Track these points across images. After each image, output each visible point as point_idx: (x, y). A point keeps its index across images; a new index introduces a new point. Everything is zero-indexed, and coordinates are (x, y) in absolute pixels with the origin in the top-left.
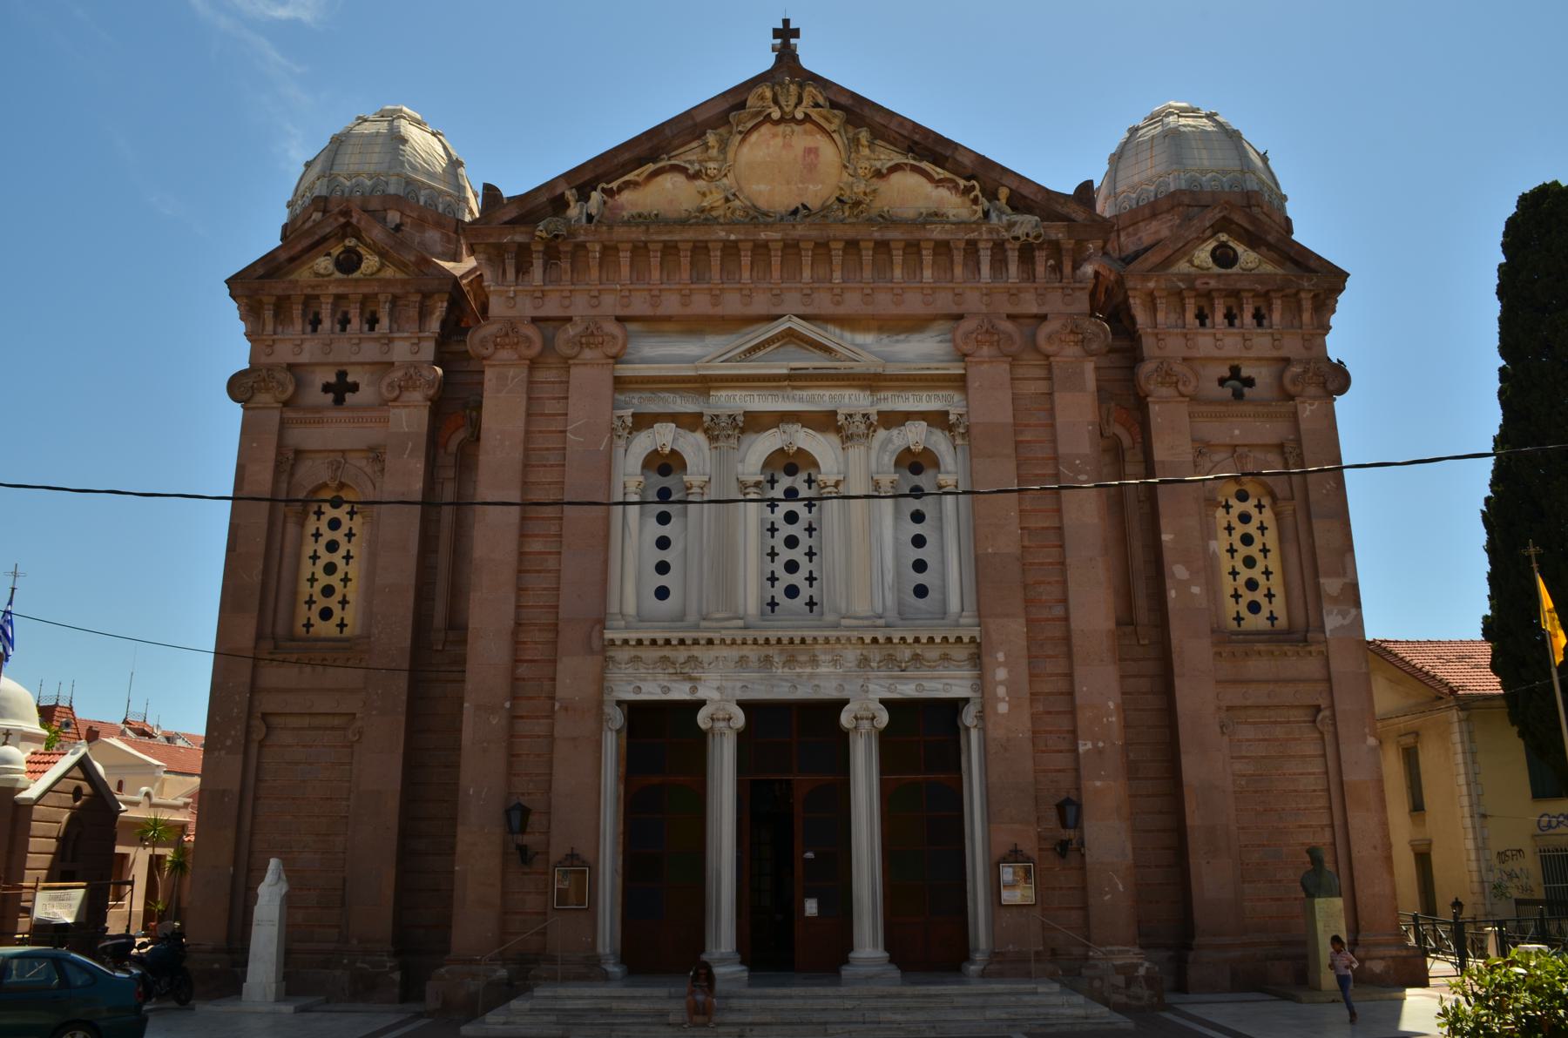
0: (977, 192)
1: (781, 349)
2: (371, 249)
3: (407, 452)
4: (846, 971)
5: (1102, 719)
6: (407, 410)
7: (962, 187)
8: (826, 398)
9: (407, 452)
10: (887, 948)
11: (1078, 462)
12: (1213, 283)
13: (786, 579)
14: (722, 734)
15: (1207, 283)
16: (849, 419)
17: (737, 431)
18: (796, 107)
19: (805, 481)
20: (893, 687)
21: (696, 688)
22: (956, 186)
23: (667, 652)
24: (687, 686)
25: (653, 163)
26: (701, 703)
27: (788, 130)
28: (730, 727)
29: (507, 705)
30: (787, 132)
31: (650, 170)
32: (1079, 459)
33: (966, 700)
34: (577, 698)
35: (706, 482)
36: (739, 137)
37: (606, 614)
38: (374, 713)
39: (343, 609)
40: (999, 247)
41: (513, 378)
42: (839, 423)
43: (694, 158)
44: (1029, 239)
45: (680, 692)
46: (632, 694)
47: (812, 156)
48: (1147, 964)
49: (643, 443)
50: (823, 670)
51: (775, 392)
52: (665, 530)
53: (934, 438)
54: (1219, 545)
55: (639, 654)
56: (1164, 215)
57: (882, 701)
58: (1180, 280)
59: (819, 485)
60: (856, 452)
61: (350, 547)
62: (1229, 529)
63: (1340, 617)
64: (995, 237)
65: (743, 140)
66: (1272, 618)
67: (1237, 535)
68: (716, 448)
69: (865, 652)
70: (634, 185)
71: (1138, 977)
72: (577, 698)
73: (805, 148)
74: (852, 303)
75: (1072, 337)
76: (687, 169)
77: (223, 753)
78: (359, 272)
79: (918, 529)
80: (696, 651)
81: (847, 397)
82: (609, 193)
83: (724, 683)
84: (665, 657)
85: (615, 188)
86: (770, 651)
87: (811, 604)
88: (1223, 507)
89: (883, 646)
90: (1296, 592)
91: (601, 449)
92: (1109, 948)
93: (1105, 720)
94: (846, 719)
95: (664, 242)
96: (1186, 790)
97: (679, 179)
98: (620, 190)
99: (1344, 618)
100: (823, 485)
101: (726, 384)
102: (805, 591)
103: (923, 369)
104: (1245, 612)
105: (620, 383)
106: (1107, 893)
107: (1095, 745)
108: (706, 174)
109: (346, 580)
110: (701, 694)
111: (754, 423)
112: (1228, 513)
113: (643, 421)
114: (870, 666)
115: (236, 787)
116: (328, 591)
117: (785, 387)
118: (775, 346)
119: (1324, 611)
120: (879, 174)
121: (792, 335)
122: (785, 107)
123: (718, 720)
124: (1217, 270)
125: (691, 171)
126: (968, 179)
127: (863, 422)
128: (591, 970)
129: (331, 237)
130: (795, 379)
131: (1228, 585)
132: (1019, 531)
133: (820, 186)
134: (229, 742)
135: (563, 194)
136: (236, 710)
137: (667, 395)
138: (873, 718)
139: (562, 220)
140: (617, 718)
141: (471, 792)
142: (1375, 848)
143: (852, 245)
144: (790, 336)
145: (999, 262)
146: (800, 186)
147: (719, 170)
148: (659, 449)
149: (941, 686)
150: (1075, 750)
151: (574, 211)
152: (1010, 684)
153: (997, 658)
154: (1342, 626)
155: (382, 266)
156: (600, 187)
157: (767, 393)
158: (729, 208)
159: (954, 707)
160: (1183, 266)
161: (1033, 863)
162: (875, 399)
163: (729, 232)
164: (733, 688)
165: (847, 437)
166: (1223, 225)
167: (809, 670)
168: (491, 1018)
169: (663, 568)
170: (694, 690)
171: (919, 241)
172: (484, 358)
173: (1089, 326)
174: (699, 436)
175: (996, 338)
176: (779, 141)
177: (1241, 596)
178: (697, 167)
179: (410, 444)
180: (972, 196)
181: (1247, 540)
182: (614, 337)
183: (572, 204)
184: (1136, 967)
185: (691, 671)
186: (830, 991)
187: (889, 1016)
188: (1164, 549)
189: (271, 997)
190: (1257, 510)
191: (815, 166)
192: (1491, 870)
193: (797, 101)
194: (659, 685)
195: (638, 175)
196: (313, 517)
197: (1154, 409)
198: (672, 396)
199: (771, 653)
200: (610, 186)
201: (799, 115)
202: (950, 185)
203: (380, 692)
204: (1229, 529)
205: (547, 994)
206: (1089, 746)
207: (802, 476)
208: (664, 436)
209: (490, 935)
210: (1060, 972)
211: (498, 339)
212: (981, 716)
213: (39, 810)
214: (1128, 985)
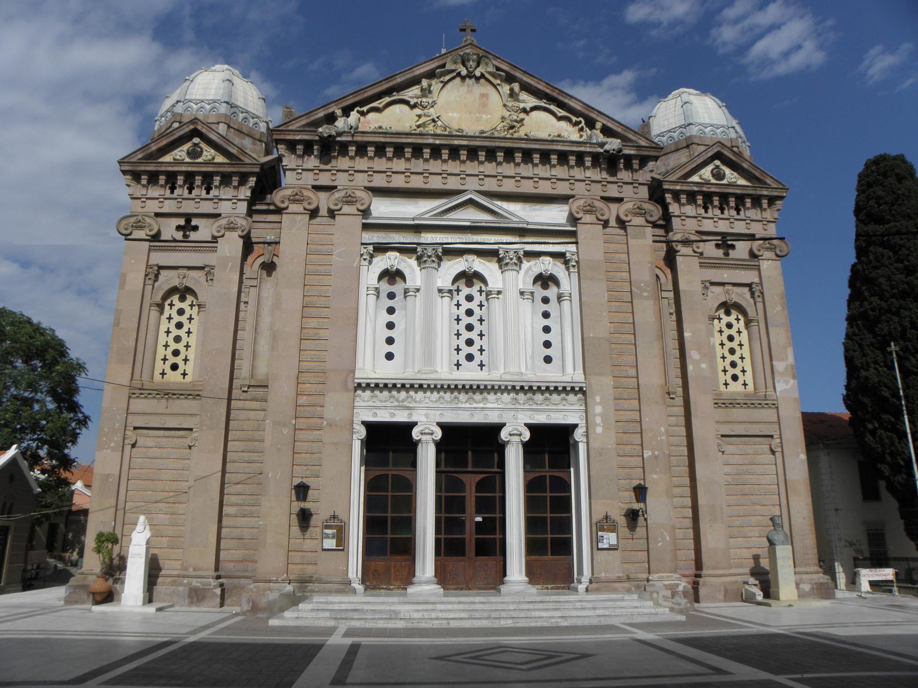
0: (583, 124)
4: (503, 588)
7: (574, 121)
11: (642, 285)
12: (713, 189)
13: (466, 350)
18: (476, 68)
19: (478, 291)
24: (406, 413)
25: (389, 97)
26: (414, 424)
32: (643, 283)
34: (337, 419)
38: (205, 428)
39: (185, 364)
42: (500, 256)
47: (485, 98)
48: (683, 584)
52: (391, 318)
54: (717, 339)
57: (527, 425)
60: (510, 275)
61: (190, 326)
62: (721, 332)
63: (784, 384)
66: (745, 385)
67: (725, 335)
70: (377, 110)
71: (679, 591)
72: (337, 419)
77: (109, 451)
78: (201, 158)
79: (546, 322)
82: (363, 114)
85: (365, 111)
88: (717, 319)
90: (760, 369)
91: (355, 266)
92: (661, 574)
94: (504, 435)
96: (698, 483)
97: (405, 108)
98: (369, 111)
99: (787, 385)
102: (478, 358)
104: (730, 381)
106: (660, 541)
107: (653, 453)
109: (187, 346)
112: (720, 322)
113: (381, 249)
115: (117, 473)
116: (176, 353)
120: (524, 111)
124: (713, 181)
125: (412, 103)
128: (345, 587)
129: (188, 123)
131: (720, 364)
133: (489, 116)
134: (113, 444)
136: (117, 424)
140: (362, 432)
141: (270, 476)
142: (804, 518)
144: (471, 202)
146: (477, 115)
150: (643, 456)
152: (603, 415)
153: (595, 400)
154: (786, 390)
156: (356, 109)
159: (569, 429)
160: (695, 178)
166: (718, 156)
168: (287, 614)
169: (390, 341)
170: (410, 415)
173: (648, 206)
177: (727, 371)
179: (230, 264)
180: (580, 126)
181: (731, 338)
184: (677, 585)
186: (493, 599)
187: (537, 614)
188: (686, 341)
189: (140, 602)
190: (736, 321)
192: (840, 540)
194: (389, 412)
195: (380, 103)
197: (679, 259)
200: (362, 109)
201: (478, 73)
203: (208, 415)
204: (721, 332)
205: (322, 600)
206: (650, 453)
207: (476, 288)
208: (391, 260)
209: (281, 564)
210: (633, 589)
214: (673, 596)
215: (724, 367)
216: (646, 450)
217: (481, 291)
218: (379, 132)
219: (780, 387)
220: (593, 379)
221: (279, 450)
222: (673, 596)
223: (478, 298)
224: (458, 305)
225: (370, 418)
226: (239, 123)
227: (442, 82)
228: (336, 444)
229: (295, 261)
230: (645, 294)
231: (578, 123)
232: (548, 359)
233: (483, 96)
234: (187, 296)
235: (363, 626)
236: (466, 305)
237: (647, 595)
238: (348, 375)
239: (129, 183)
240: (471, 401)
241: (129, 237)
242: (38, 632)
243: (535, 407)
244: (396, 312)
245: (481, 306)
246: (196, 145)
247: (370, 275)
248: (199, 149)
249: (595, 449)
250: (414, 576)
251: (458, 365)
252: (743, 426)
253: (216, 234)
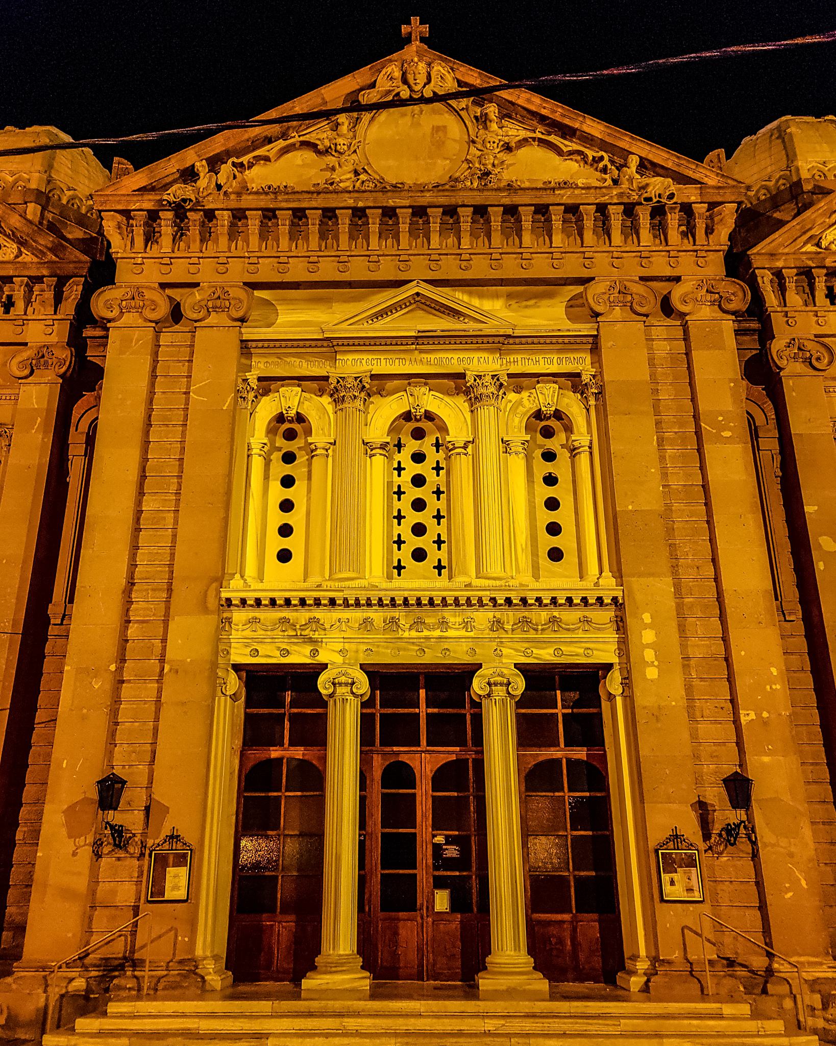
0: (606, 161)
1: (407, 315)
2: (10, 238)
3: (36, 427)
5: (765, 687)
6: (38, 387)
8: (455, 361)
9: (36, 427)
10: (530, 952)
11: (720, 418)
13: (413, 542)
14: (344, 701)
16: (478, 381)
17: (363, 394)
20: (529, 651)
21: (317, 651)
22: (585, 157)
23: (286, 613)
24: (307, 649)
28: (352, 693)
29: (113, 667)
30: (416, 112)
31: (279, 147)
33: (608, 667)
35: (331, 443)
37: (224, 573)
40: (629, 210)
41: (138, 341)
42: (468, 385)
43: (325, 135)
44: (662, 200)
45: (300, 656)
46: (249, 657)
47: (440, 134)
49: (267, 409)
50: (451, 633)
51: (402, 356)
52: (289, 493)
55: (257, 615)
56: (786, 206)
59: (447, 448)
64: (626, 200)
68: (341, 410)
69: (498, 615)
73: (433, 126)
74: (480, 268)
75: (709, 297)
76: (317, 145)
80: (319, 614)
81: (476, 360)
83: (347, 646)
84: (285, 618)
85: (245, 163)
86: (395, 613)
87: (439, 567)
89: (212, 593)
91: (225, 408)
94: (478, 686)
95: (293, 209)
97: (308, 155)
98: (251, 165)
100: (451, 447)
101: (353, 348)
103: (553, 331)
105: (246, 347)
106: (788, 890)
107: (758, 715)
108: (336, 151)
110: (322, 658)
113: (267, 384)
114: (503, 629)
120: (508, 148)
122: (413, 85)
123: (340, 684)
127: (493, 383)
130: (422, 340)
132: (661, 488)
135: (193, 166)
137: (293, 359)
138: (509, 684)
139: (190, 188)
141: (64, 766)
143: (481, 211)
144: (421, 303)
145: (632, 229)
147: (349, 147)
148: (284, 412)
149: (582, 651)
151: (202, 183)
155: (20, 253)
156: (230, 161)
157: (394, 356)
158: (358, 179)
161: (697, 850)
162: (505, 361)
163: (356, 200)
164: (357, 651)
165: (476, 398)
167: (437, 633)
170: (315, 653)
171: (548, 206)
172: (109, 321)
174: (326, 400)
175: (629, 298)
176: (408, 120)
178: (327, 143)
182: (241, 301)
183: (202, 175)
185: (312, 633)
191: (443, 143)
193: (425, 80)
198: (298, 360)
199: (397, 615)
202: (579, 158)
206: (753, 716)
210: (742, 989)
211: (124, 303)
212: (627, 682)
213: (293, 830)
216: (744, 709)
217: (437, 445)
218: (268, 191)
220: (636, 583)
221: (84, 718)
223: (432, 456)
224: (399, 469)
226: (63, 206)
228: (184, 704)
229: (129, 402)
230: (727, 434)
231: (598, 160)
232: (556, 555)
233: (437, 129)
235: (366, 848)
236: (412, 469)
237: (769, 1004)
240: (420, 627)
242: (582, 640)
243: (532, 635)
244: (296, 482)
245: (438, 469)
249: (645, 708)
250: (319, 952)
251: (399, 568)
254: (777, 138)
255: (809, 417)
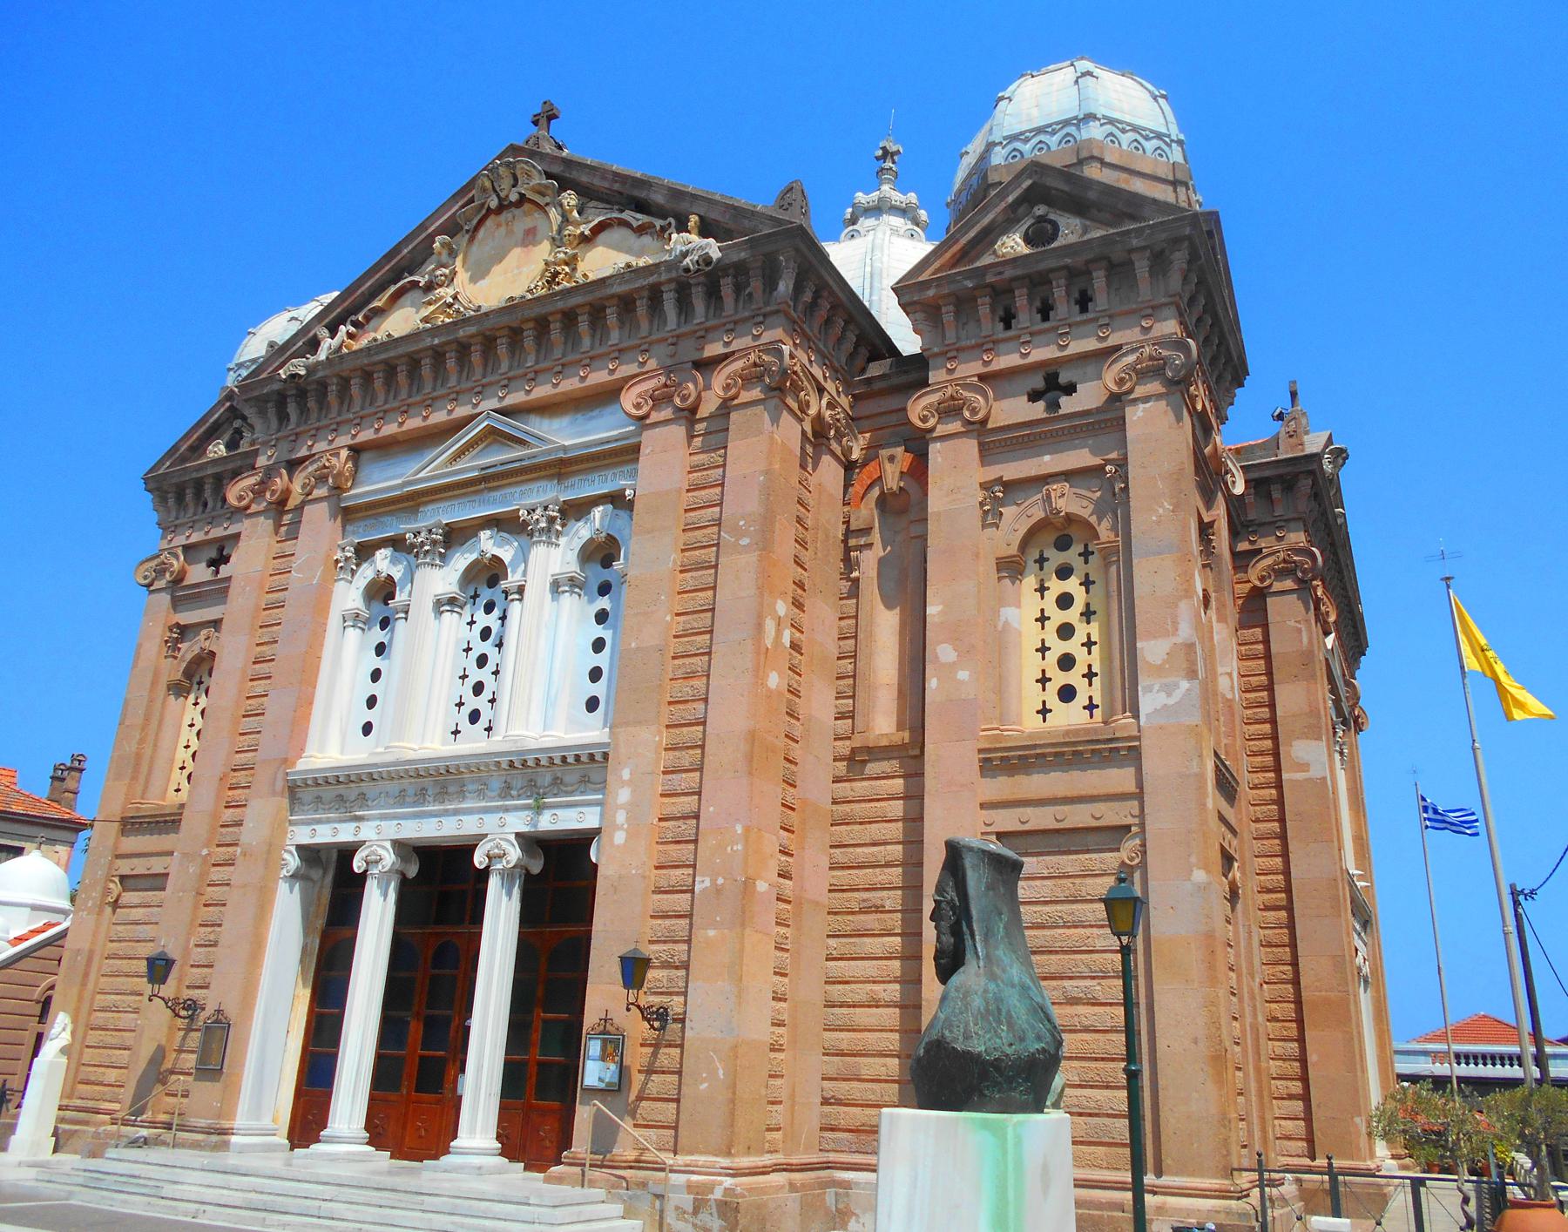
11: (741, 523)
15: (1000, 273)
23: (341, 789)
27: (510, 215)
36: (467, 236)
51: (473, 498)
53: (619, 523)
58: (966, 279)
63: (1163, 695)
65: (472, 239)
71: (709, 1200)
90: (1117, 663)
93: (729, 848)
94: (479, 860)
98: (368, 319)
99: (1169, 695)
104: (1053, 701)
107: (713, 882)
111: (455, 536)
117: (482, 490)
118: (481, 447)
119: (1140, 688)
121: (494, 433)
126: (665, 218)
140: (293, 862)
145: (684, 305)
152: (632, 808)
193: (512, 182)
196: (196, 686)
198: (390, 519)
206: (707, 883)
214: (696, 1211)
215: (1043, 671)
219: (1150, 701)
222: (696, 1211)
225: (306, 840)
227: (467, 231)
230: (745, 541)
231: (663, 229)
234: (897, 610)
238: (278, 768)
239: (920, 326)
241: (152, 588)
246: (1041, 219)
247: (349, 595)
248: (1049, 227)
252: (1049, 811)
253: (1115, 388)
254: (1079, 129)
255: (952, 487)
